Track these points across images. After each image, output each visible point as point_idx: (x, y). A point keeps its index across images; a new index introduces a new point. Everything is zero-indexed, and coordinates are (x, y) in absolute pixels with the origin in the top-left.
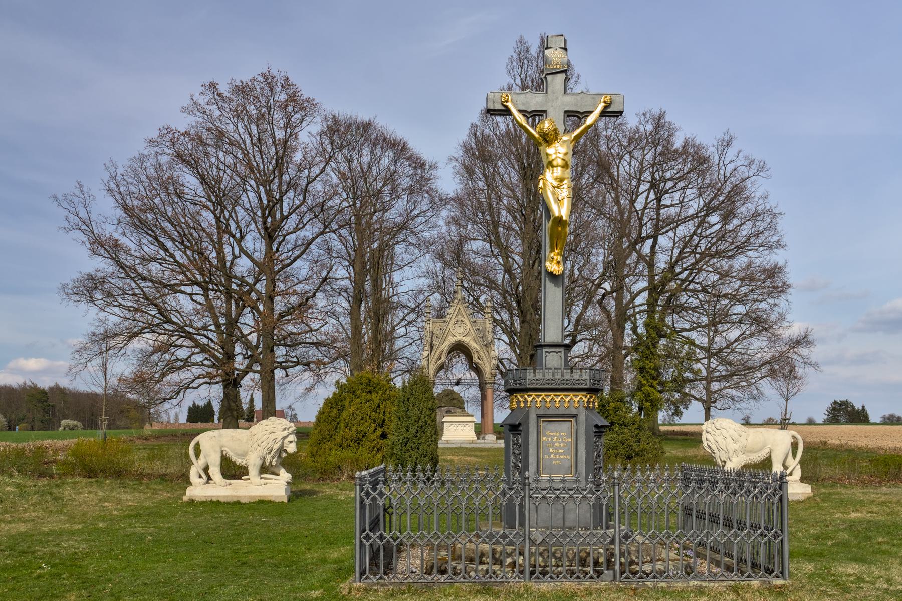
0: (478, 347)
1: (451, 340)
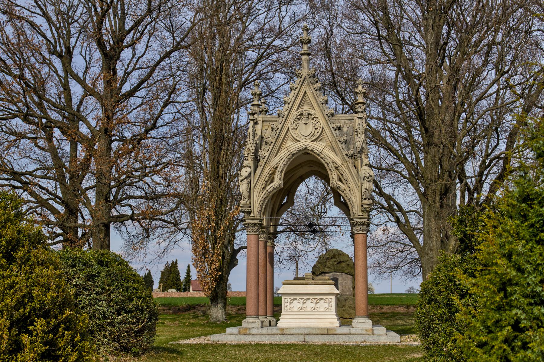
0: (338, 160)
1: (292, 147)
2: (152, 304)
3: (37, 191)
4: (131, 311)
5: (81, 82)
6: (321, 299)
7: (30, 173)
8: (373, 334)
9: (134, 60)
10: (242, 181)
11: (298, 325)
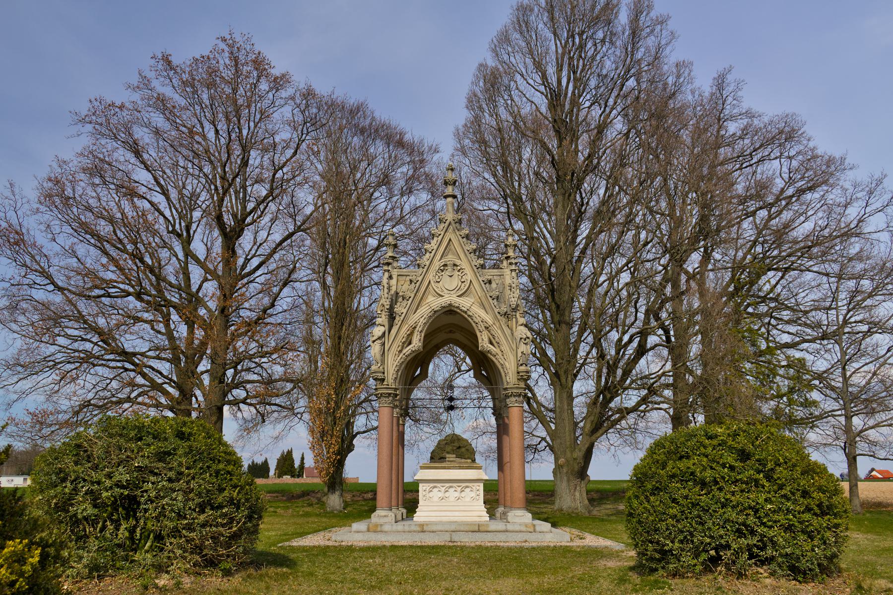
0: (489, 319)
1: (433, 303)
2: (253, 496)
3: (152, 374)
4: (220, 507)
5: (201, 264)
6: (467, 487)
7: (143, 354)
8: (535, 531)
9: (256, 247)
10: (374, 342)
11: (439, 519)
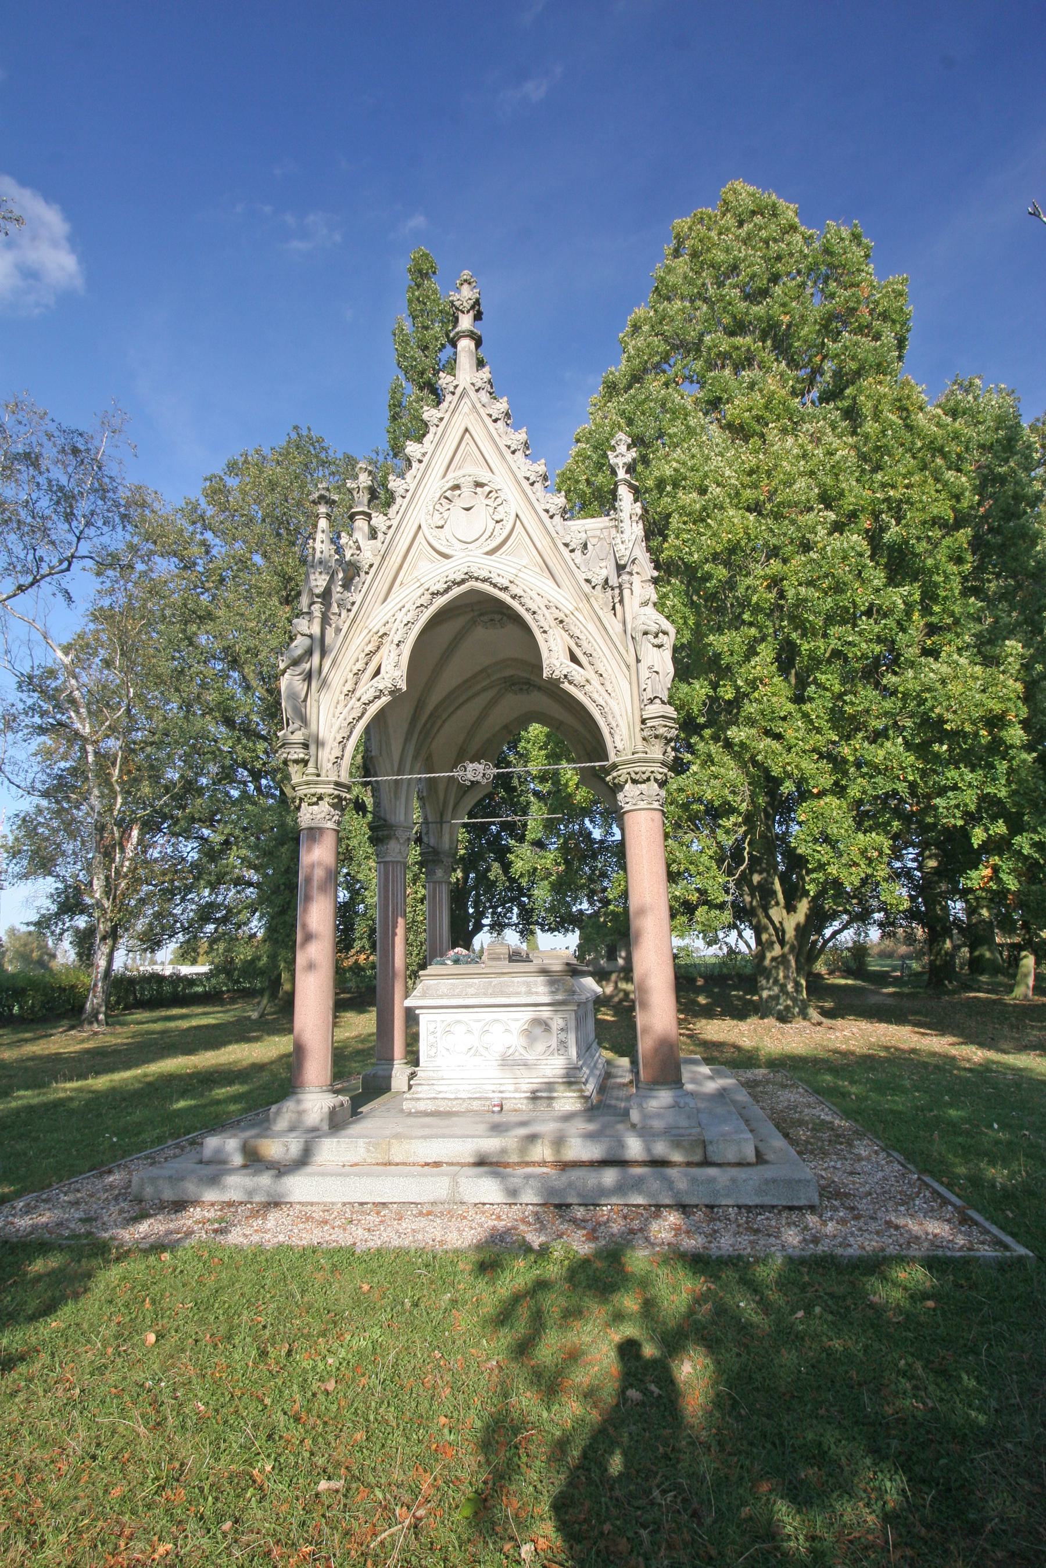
0: (565, 599)
